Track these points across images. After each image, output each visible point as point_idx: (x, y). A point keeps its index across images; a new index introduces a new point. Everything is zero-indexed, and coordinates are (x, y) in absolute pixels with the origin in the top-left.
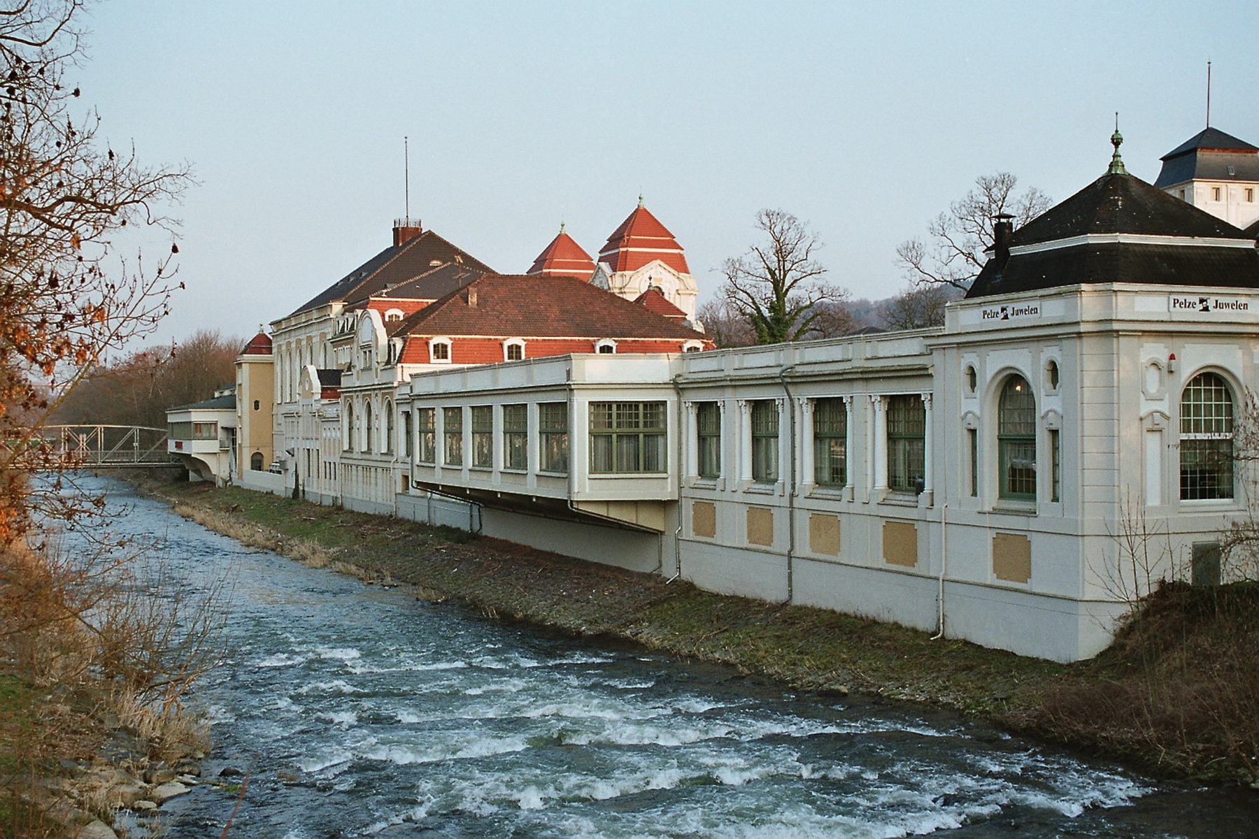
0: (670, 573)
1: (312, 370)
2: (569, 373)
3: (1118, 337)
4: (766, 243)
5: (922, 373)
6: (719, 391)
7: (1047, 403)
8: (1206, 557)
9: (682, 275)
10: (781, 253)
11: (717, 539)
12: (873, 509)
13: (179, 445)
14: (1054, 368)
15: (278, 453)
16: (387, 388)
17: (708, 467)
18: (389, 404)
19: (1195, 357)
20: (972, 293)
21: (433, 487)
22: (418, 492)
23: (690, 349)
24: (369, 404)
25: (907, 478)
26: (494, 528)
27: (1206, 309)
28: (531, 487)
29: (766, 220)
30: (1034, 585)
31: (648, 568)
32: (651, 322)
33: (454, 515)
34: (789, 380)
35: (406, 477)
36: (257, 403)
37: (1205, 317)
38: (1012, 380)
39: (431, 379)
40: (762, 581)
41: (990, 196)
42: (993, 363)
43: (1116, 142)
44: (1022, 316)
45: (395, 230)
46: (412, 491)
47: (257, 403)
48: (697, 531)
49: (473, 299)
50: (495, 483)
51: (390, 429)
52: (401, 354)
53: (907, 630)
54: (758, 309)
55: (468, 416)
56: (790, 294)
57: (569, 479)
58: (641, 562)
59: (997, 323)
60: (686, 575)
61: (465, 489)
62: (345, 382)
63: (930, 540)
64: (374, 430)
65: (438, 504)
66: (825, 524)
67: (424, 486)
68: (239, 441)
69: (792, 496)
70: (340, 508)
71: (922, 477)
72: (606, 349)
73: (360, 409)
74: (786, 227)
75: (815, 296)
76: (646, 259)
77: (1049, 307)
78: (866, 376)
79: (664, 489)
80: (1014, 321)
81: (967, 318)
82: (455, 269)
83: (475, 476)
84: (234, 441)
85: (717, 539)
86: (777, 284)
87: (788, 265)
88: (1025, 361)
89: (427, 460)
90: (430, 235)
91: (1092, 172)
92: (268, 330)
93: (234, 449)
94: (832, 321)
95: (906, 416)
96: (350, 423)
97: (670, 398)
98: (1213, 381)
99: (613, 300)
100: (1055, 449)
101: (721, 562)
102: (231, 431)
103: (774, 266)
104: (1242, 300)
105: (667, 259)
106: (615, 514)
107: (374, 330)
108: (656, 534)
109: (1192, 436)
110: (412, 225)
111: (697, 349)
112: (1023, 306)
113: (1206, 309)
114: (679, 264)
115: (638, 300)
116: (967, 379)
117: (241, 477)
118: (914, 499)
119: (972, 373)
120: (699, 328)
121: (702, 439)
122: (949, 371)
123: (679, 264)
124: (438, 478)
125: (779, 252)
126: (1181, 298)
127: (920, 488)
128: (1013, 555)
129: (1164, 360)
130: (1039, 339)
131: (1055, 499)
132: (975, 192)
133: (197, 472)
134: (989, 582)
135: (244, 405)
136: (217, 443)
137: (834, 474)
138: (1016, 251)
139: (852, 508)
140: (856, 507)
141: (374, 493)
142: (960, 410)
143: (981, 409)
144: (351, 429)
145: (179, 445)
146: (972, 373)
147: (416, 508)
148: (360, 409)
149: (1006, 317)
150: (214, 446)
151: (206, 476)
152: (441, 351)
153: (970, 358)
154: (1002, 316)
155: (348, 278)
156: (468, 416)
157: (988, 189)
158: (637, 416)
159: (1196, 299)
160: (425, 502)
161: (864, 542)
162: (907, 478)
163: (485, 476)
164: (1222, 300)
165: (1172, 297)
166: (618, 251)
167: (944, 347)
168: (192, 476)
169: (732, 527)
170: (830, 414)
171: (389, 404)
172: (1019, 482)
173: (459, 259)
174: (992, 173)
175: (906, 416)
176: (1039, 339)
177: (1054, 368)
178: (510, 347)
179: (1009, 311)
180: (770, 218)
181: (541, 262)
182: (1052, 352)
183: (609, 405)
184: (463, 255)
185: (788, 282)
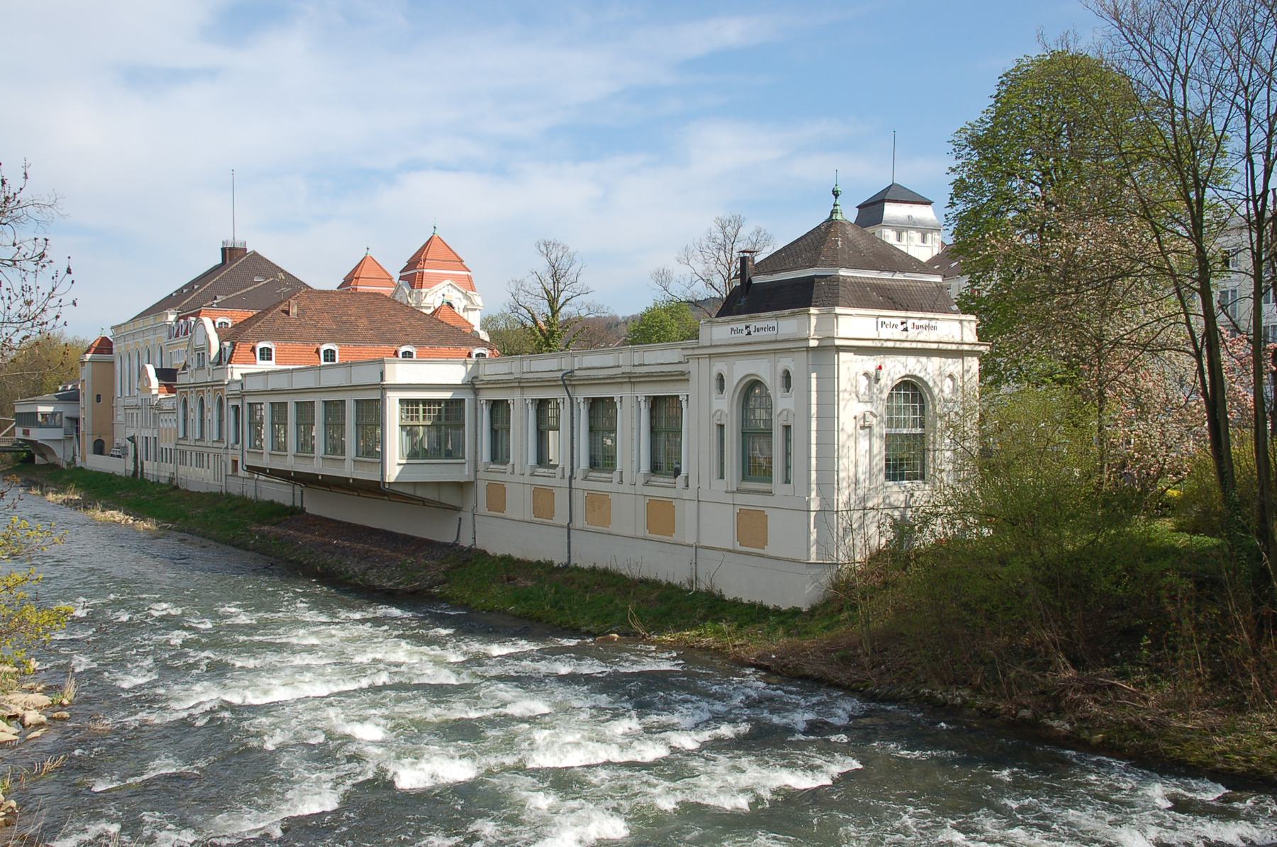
0: (466, 542)
1: (151, 370)
2: (382, 374)
3: (838, 352)
4: (542, 265)
5: (682, 377)
6: (509, 391)
7: (783, 403)
8: (902, 529)
9: (470, 293)
10: (556, 277)
11: (507, 514)
12: (527, 479)
13: (26, 433)
14: (787, 376)
15: (118, 440)
16: (217, 385)
17: (499, 454)
18: (221, 399)
19: (896, 368)
20: (721, 314)
21: (261, 470)
22: (247, 474)
23: (478, 355)
24: (202, 400)
25: (664, 463)
26: (316, 505)
27: (906, 330)
28: (348, 469)
29: (543, 248)
30: (768, 550)
31: (450, 539)
32: (442, 333)
33: (281, 493)
34: (568, 381)
35: (235, 462)
36: (98, 397)
37: (749, 339)
38: (752, 387)
39: (261, 378)
40: (543, 546)
41: (724, 233)
42: (738, 371)
43: (836, 194)
44: (762, 333)
45: (224, 250)
46: (241, 473)
47: (98, 397)
48: (490, 508)
49: (294, 310)
50: (317, 466)
51: (220, 421)
52: (231, 356)
53: (587, 571)
54: (535, 321)
55: (292, 410)
56: (562, 310)
57: (382, 463)
58: (443, 533)
59: (742, 337)
60: (480, 545)
61: (289, 472)
62: (181, 379)
63: (685, 514)
64: (189, 421)
65: (264, 486)
66: (598, 503)
67: (251, 469)
68: (82, 429)
69: (571, 478)
70: (176, 488)
71: (680, 463)
72: (407, 355)
73: (193, 404)
74: (560, 255)
75: (584, 313)
76: (440, 279)
77: (785, 325)
78: (631, 380)
79: (464, 474)
80: (756, 336)
81: (721, 332)
82: (280, 284)
83: (299, 460)
84: (78, 430)
85: (507, 514)
86: (552, 302)
87: (561, 286)
88: (764, 369)
89: (334, 451)
90: (255, 254)
91: (817, 219)
92: (108, 334)
93: (78, 437)
94: (595, 333)
95: (663, 412)
96: (185, 415)
97: (468, 397)
98: (912, 389)
99: (415, 312)
100: (787, 440)
101: (510, 532)
102: (75, 421)
103: (550, 286)
104: (933, 323)
105: (457, 279)
106: (420, 493)
107: (207, 336)
108: (457, 509)
109: (893, 431)
110: (238, 246)
111: (483, 355)
112: (760, 324)
113: (906, 330)
114: (469, 284)
115: (433, 313)
116: (714, 383)
117: (84, 459)
118: (672, 480)
119: (721, 379)
120: (485, 336)
121: (494, 432)
122: (704, 374)
123: (470, 284)
124: (266, 462)
125: (554, 275)
126: (887, 320)
127: (677, 472)
128: (752, 528)
129: (872, 370)
130: (775, 351)
131: (787, 481)
132: (714, 229)
133: (43, 455)
134: (527, 519)
135: (86, 401)
136: (61, 431)
137: (602, 461)
138: (757, 280)
139: (621, 488)
140: (625, 487)
141: (201, 476)
142: (707, 411)
143: (725, 406)
144: (185, 421)
145: (26, 433)
146: (721, 379)
147: (243, 486)
148: (193, 404)
149: (749, 333)
150: (58, 434)
151: (51, 459)
152: (266, 355)
153: (720, 366)
154: (746, 332)
155: (181, 290)
156: (292, 410)
157: (723, 228)
158: (417, 411)
159: (898, 321)
160: (252, 483)
161: (627, 513)
162: (664, 463)
163: (308, 461)
164: (918, 323)
165: (880, 320)
166: (413, 273)
167: (698, 357)
168: (38, 460)
169: (519, 503)
170: (601, 410)
171: (221, 399)
172: (754, 469)
173: (281, 275)
174: (725, 215)
175: (663, 412)
176: (775, 351)
177: (787, 376)
178: (326, 351)
179: (752, 329)
180: (547, 247)
181: (348, 281)
182: (786, 362)
183: (416, 402)
184: (185, 287)
185: (561, 300)
